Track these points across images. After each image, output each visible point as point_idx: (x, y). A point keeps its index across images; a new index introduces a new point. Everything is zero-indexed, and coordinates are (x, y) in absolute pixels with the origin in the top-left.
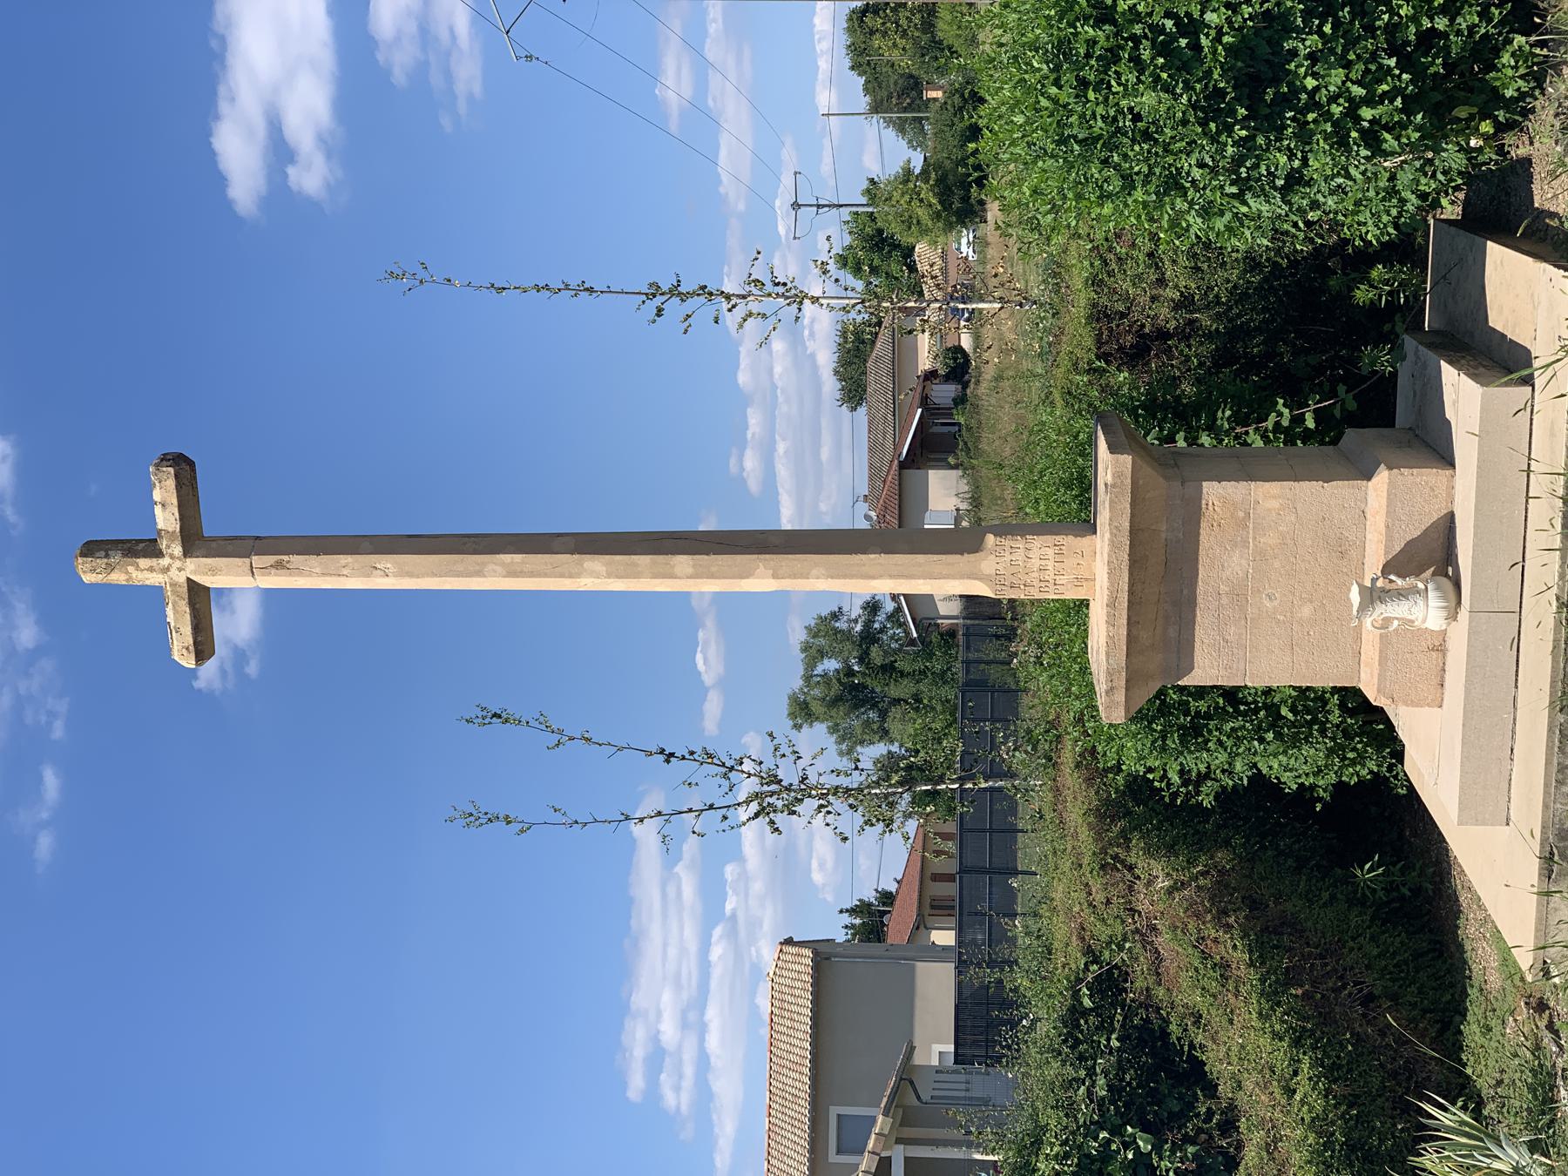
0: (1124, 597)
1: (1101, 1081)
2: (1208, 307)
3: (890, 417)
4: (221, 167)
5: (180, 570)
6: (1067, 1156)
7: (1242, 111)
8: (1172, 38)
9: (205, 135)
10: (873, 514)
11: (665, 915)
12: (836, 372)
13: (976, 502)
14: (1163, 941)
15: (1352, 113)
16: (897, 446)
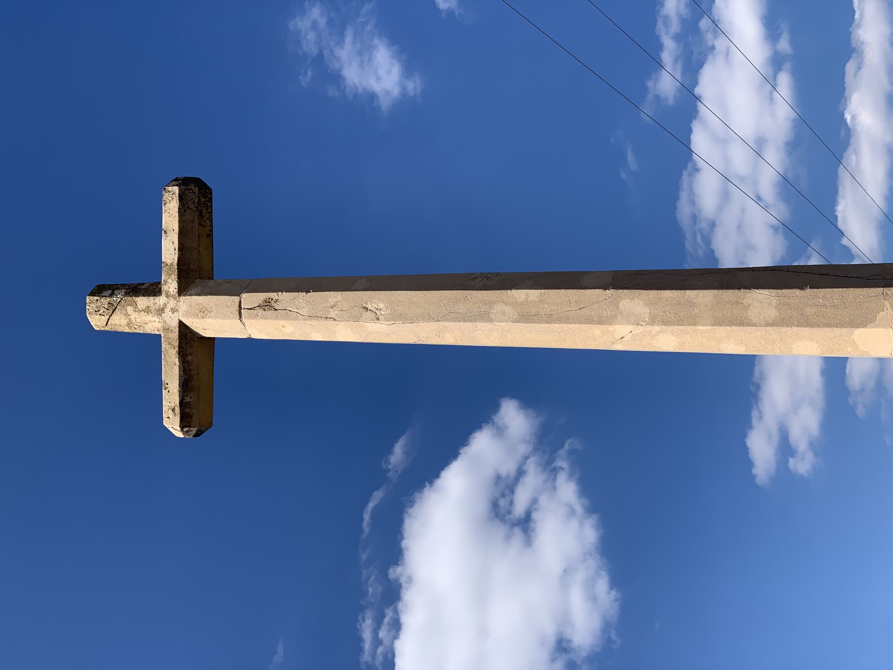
4: (750, 456)
5: (174, 310)
9: (745, 436)
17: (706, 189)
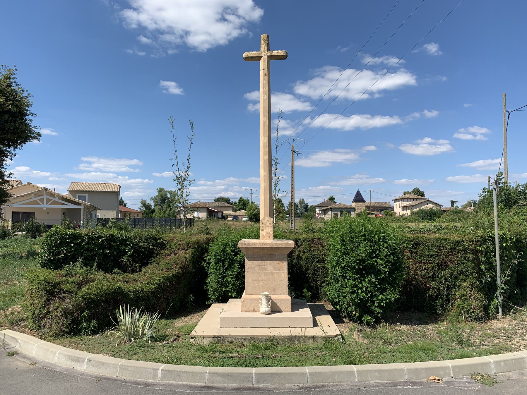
0: (265, 246)
1: (142, 244)
2: (298, 261)
6: (126, 237)
7: (361, 267)
8: (375, 253)
11: (118, 165)
13: (202, 221)
14: (172, 256)
15: (359, 288)
16: (210, 207)
17: (334, 74)
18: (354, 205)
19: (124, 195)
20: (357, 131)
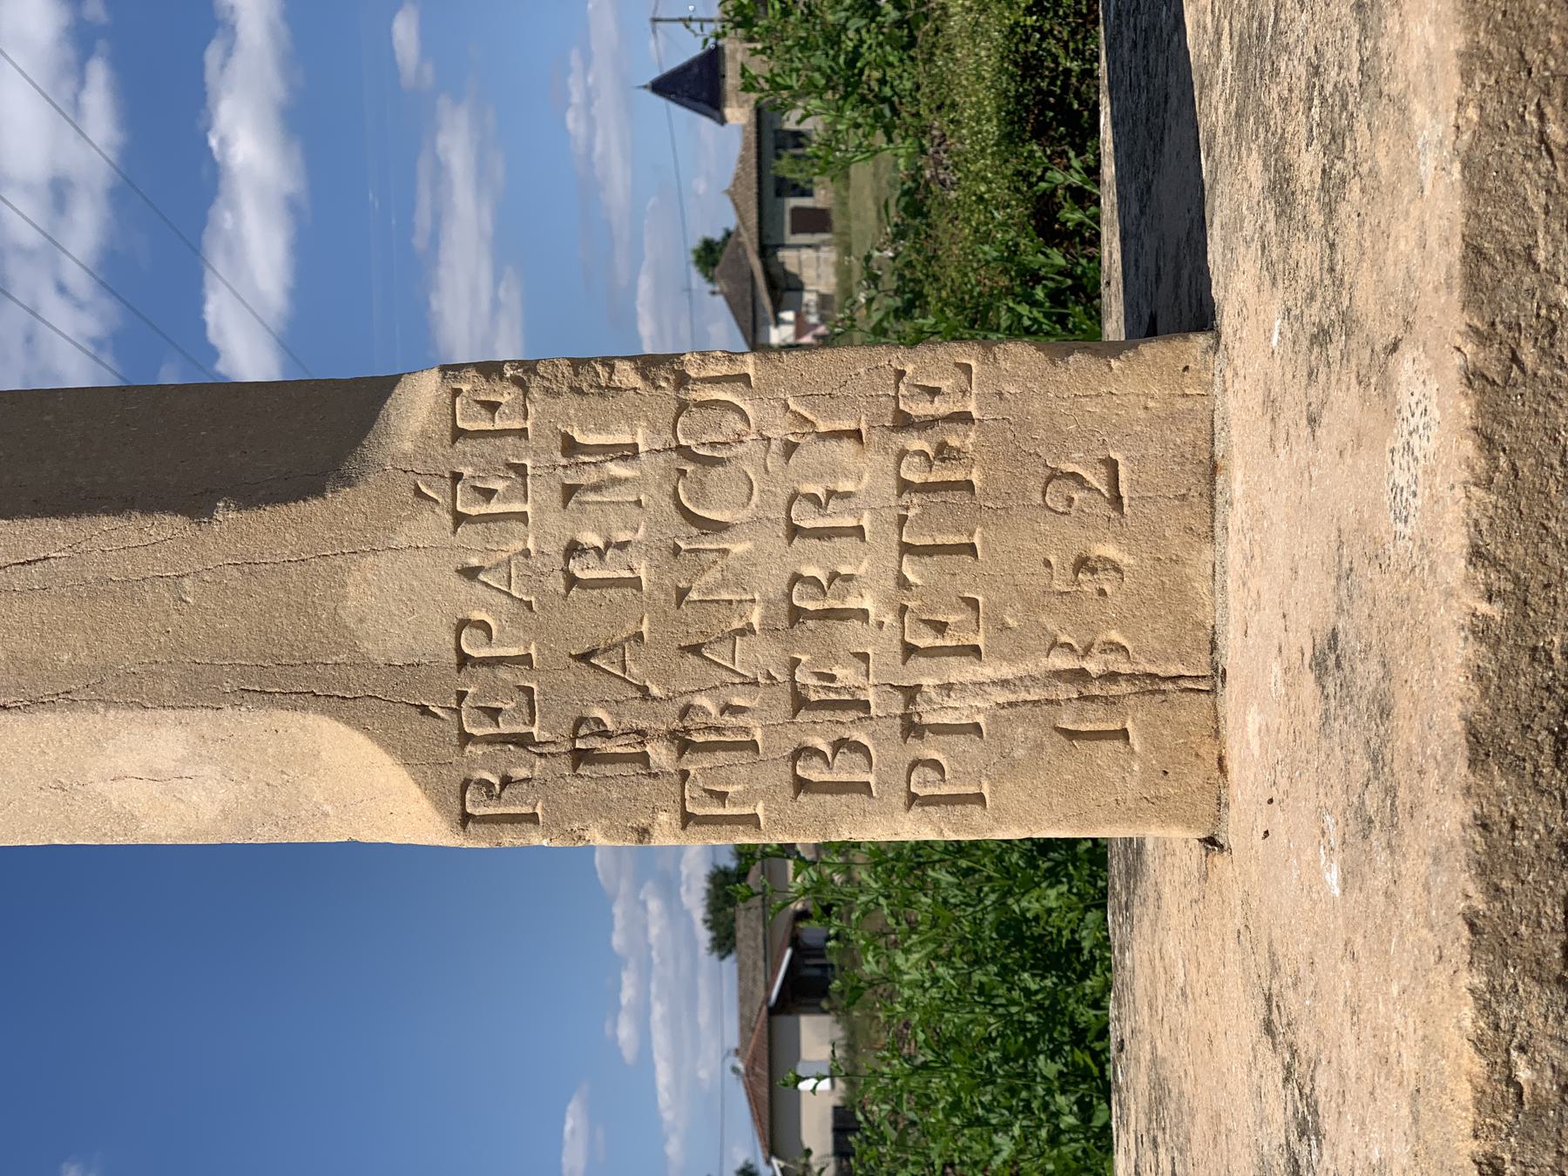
3: (761, 964)
10: (741, 1066)
12: (706, 921)
13: (851, 1047)
18: (738, 114)
19: (718, 215)
20: (305, 121)
